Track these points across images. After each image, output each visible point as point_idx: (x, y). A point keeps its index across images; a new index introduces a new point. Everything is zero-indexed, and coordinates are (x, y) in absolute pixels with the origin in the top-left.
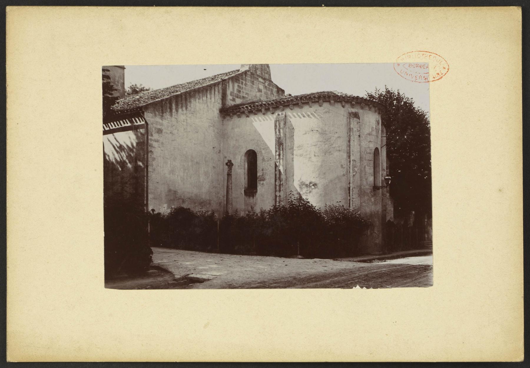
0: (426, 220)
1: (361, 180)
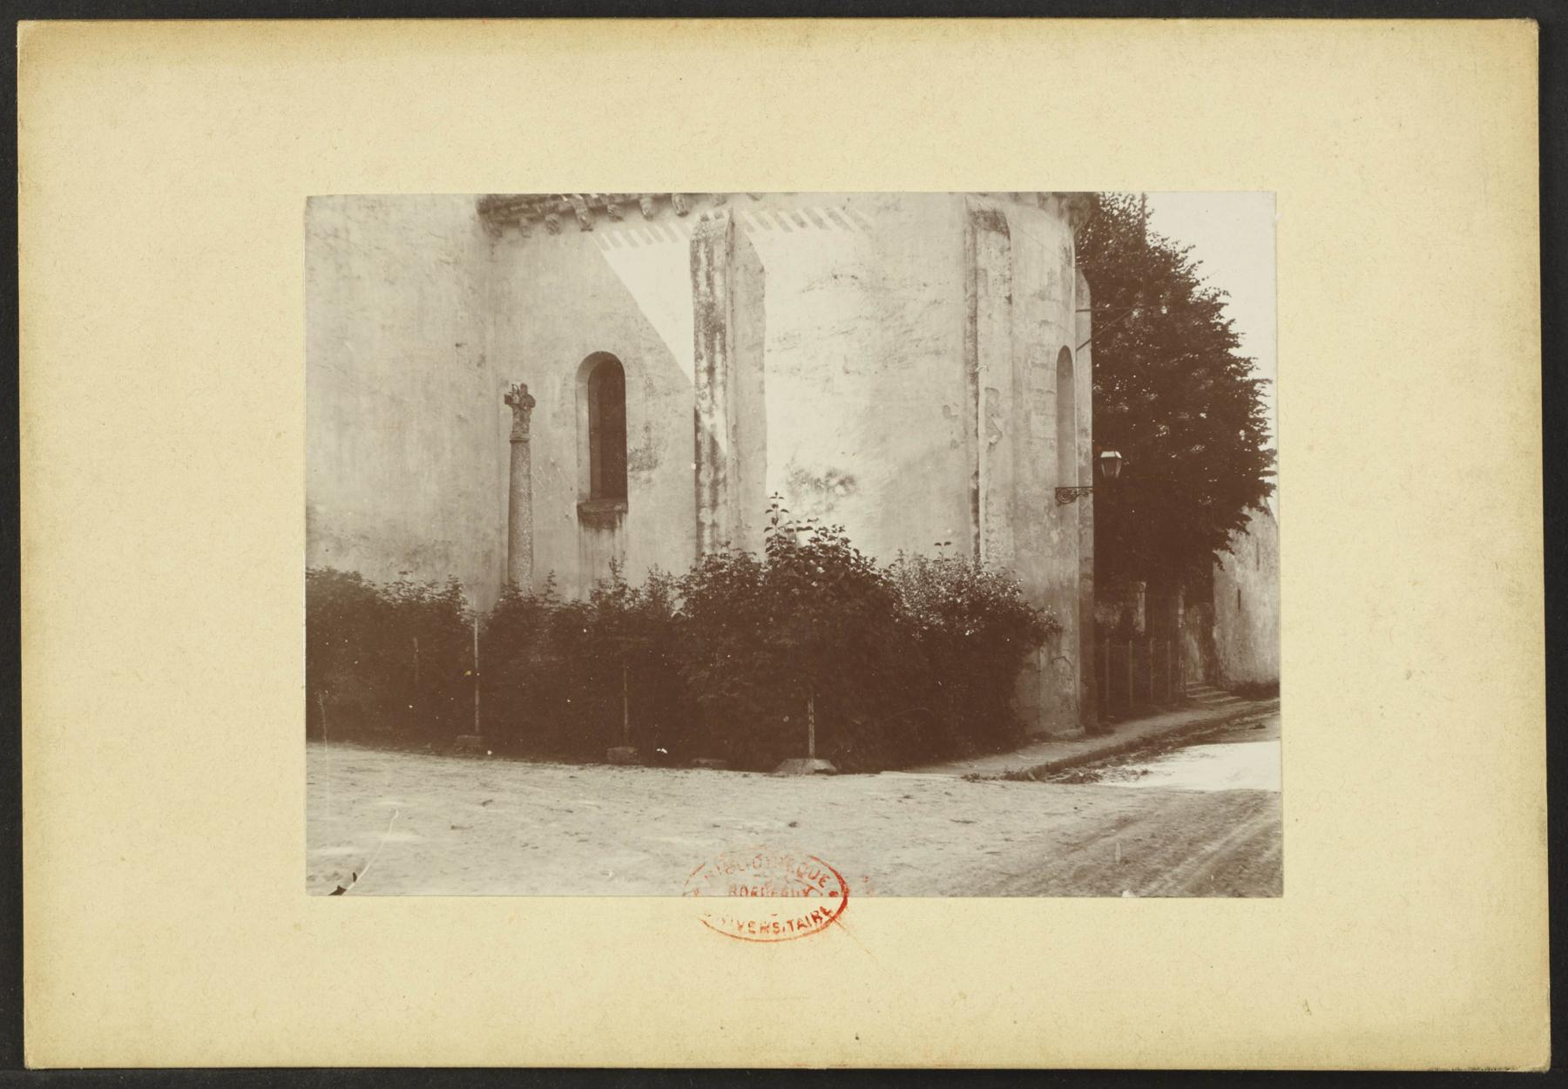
0: (1181, 612)
1: (1016, 464)
